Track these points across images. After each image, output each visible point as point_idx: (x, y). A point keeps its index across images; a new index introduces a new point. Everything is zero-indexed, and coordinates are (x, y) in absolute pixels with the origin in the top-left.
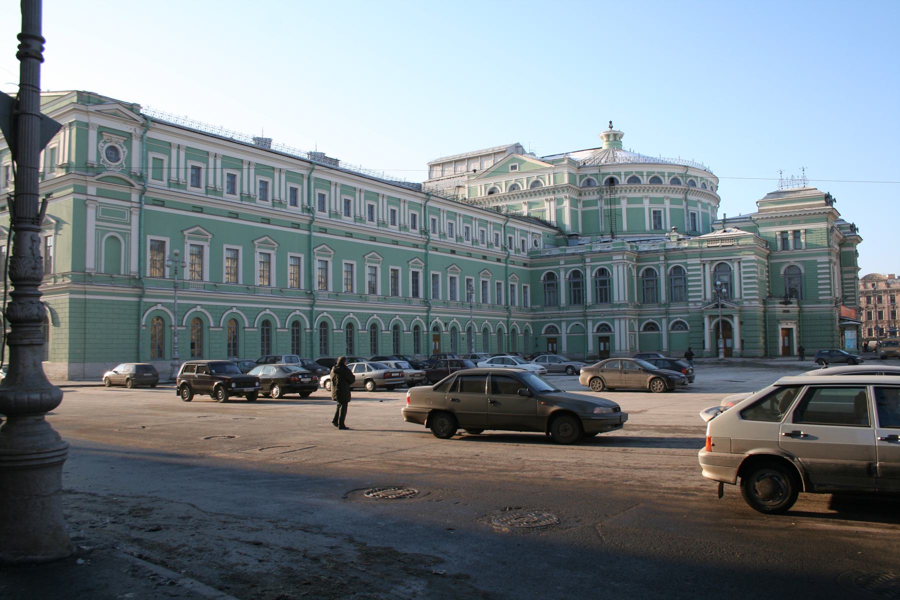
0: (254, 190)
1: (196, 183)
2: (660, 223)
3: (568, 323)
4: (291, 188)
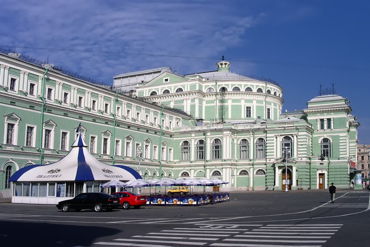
2: (250, 113)
3: (195, 170)
4: (12, 79)
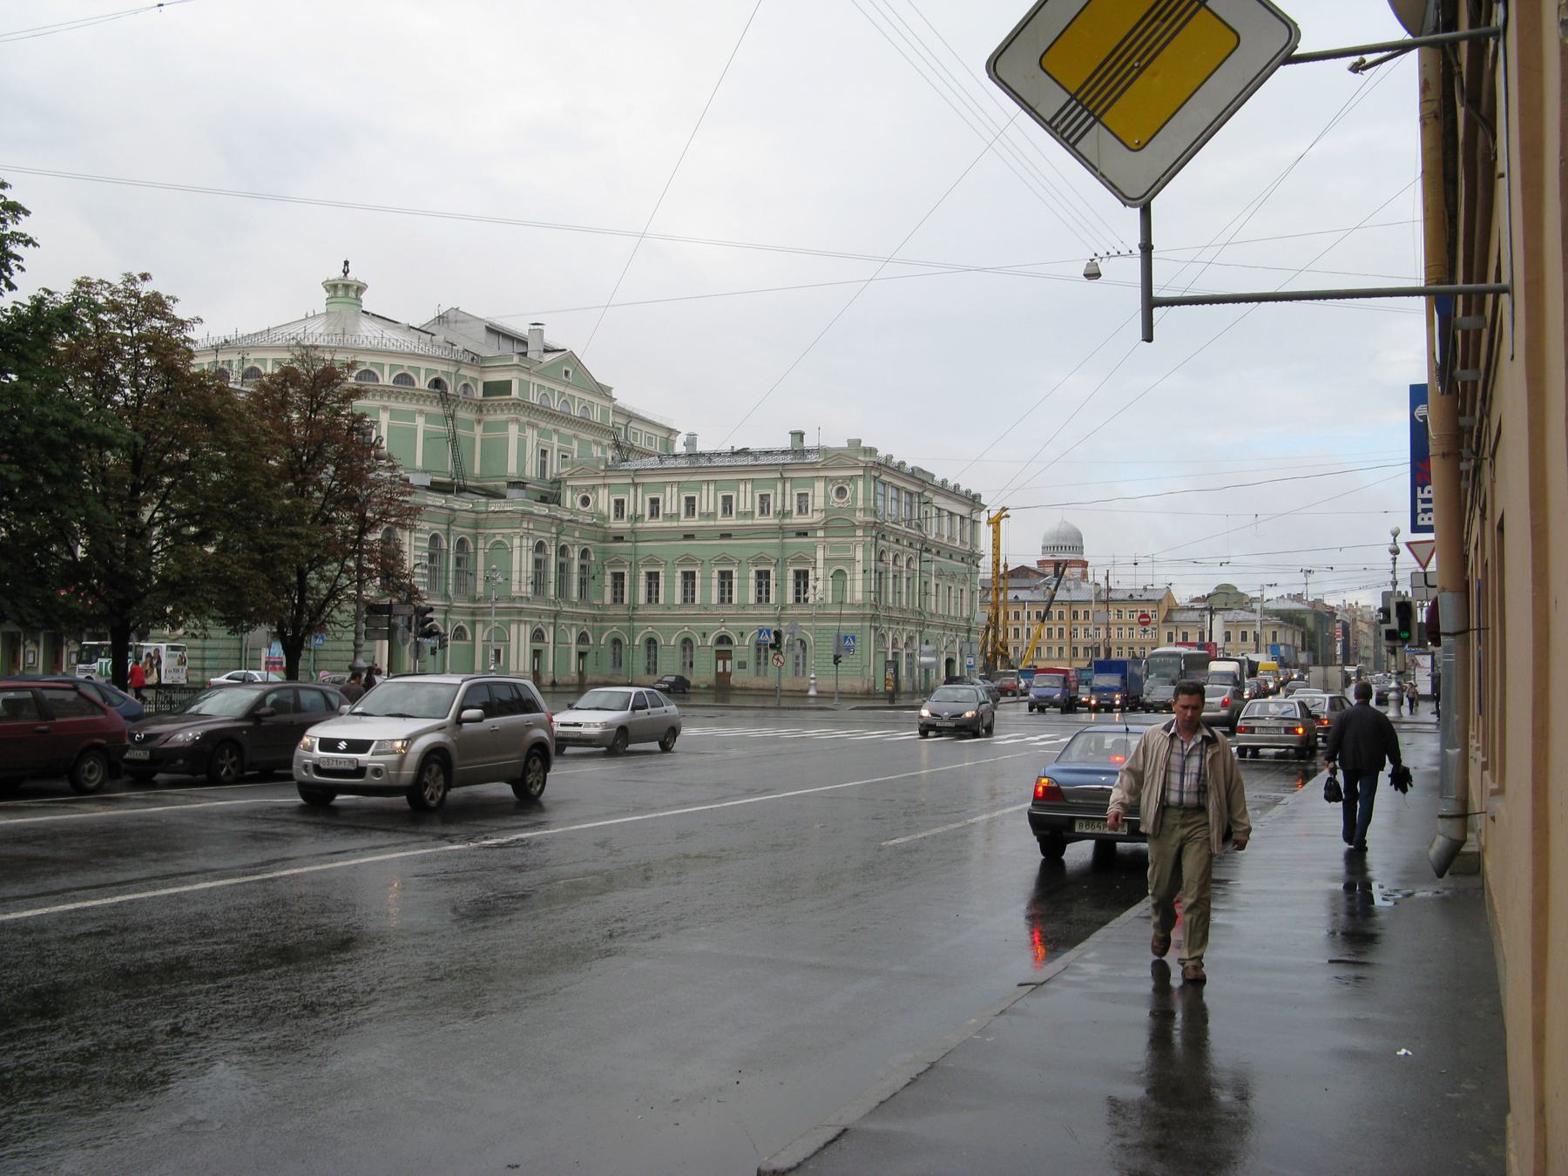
0: (792, 504)
1: (654, 513)
